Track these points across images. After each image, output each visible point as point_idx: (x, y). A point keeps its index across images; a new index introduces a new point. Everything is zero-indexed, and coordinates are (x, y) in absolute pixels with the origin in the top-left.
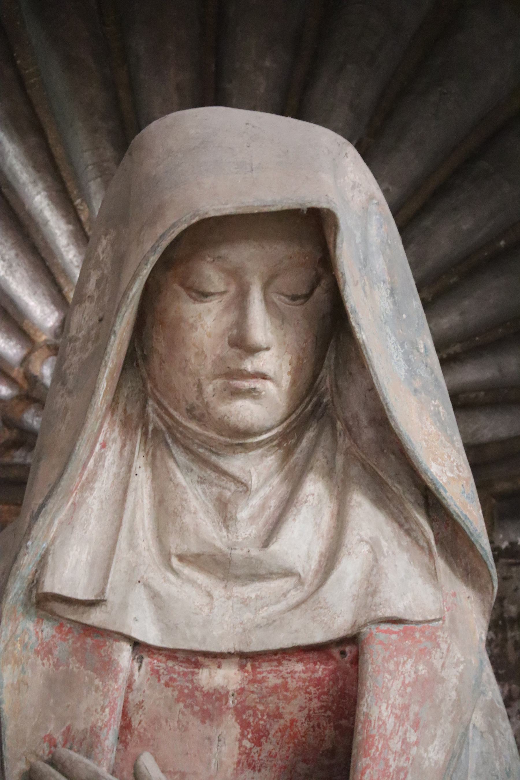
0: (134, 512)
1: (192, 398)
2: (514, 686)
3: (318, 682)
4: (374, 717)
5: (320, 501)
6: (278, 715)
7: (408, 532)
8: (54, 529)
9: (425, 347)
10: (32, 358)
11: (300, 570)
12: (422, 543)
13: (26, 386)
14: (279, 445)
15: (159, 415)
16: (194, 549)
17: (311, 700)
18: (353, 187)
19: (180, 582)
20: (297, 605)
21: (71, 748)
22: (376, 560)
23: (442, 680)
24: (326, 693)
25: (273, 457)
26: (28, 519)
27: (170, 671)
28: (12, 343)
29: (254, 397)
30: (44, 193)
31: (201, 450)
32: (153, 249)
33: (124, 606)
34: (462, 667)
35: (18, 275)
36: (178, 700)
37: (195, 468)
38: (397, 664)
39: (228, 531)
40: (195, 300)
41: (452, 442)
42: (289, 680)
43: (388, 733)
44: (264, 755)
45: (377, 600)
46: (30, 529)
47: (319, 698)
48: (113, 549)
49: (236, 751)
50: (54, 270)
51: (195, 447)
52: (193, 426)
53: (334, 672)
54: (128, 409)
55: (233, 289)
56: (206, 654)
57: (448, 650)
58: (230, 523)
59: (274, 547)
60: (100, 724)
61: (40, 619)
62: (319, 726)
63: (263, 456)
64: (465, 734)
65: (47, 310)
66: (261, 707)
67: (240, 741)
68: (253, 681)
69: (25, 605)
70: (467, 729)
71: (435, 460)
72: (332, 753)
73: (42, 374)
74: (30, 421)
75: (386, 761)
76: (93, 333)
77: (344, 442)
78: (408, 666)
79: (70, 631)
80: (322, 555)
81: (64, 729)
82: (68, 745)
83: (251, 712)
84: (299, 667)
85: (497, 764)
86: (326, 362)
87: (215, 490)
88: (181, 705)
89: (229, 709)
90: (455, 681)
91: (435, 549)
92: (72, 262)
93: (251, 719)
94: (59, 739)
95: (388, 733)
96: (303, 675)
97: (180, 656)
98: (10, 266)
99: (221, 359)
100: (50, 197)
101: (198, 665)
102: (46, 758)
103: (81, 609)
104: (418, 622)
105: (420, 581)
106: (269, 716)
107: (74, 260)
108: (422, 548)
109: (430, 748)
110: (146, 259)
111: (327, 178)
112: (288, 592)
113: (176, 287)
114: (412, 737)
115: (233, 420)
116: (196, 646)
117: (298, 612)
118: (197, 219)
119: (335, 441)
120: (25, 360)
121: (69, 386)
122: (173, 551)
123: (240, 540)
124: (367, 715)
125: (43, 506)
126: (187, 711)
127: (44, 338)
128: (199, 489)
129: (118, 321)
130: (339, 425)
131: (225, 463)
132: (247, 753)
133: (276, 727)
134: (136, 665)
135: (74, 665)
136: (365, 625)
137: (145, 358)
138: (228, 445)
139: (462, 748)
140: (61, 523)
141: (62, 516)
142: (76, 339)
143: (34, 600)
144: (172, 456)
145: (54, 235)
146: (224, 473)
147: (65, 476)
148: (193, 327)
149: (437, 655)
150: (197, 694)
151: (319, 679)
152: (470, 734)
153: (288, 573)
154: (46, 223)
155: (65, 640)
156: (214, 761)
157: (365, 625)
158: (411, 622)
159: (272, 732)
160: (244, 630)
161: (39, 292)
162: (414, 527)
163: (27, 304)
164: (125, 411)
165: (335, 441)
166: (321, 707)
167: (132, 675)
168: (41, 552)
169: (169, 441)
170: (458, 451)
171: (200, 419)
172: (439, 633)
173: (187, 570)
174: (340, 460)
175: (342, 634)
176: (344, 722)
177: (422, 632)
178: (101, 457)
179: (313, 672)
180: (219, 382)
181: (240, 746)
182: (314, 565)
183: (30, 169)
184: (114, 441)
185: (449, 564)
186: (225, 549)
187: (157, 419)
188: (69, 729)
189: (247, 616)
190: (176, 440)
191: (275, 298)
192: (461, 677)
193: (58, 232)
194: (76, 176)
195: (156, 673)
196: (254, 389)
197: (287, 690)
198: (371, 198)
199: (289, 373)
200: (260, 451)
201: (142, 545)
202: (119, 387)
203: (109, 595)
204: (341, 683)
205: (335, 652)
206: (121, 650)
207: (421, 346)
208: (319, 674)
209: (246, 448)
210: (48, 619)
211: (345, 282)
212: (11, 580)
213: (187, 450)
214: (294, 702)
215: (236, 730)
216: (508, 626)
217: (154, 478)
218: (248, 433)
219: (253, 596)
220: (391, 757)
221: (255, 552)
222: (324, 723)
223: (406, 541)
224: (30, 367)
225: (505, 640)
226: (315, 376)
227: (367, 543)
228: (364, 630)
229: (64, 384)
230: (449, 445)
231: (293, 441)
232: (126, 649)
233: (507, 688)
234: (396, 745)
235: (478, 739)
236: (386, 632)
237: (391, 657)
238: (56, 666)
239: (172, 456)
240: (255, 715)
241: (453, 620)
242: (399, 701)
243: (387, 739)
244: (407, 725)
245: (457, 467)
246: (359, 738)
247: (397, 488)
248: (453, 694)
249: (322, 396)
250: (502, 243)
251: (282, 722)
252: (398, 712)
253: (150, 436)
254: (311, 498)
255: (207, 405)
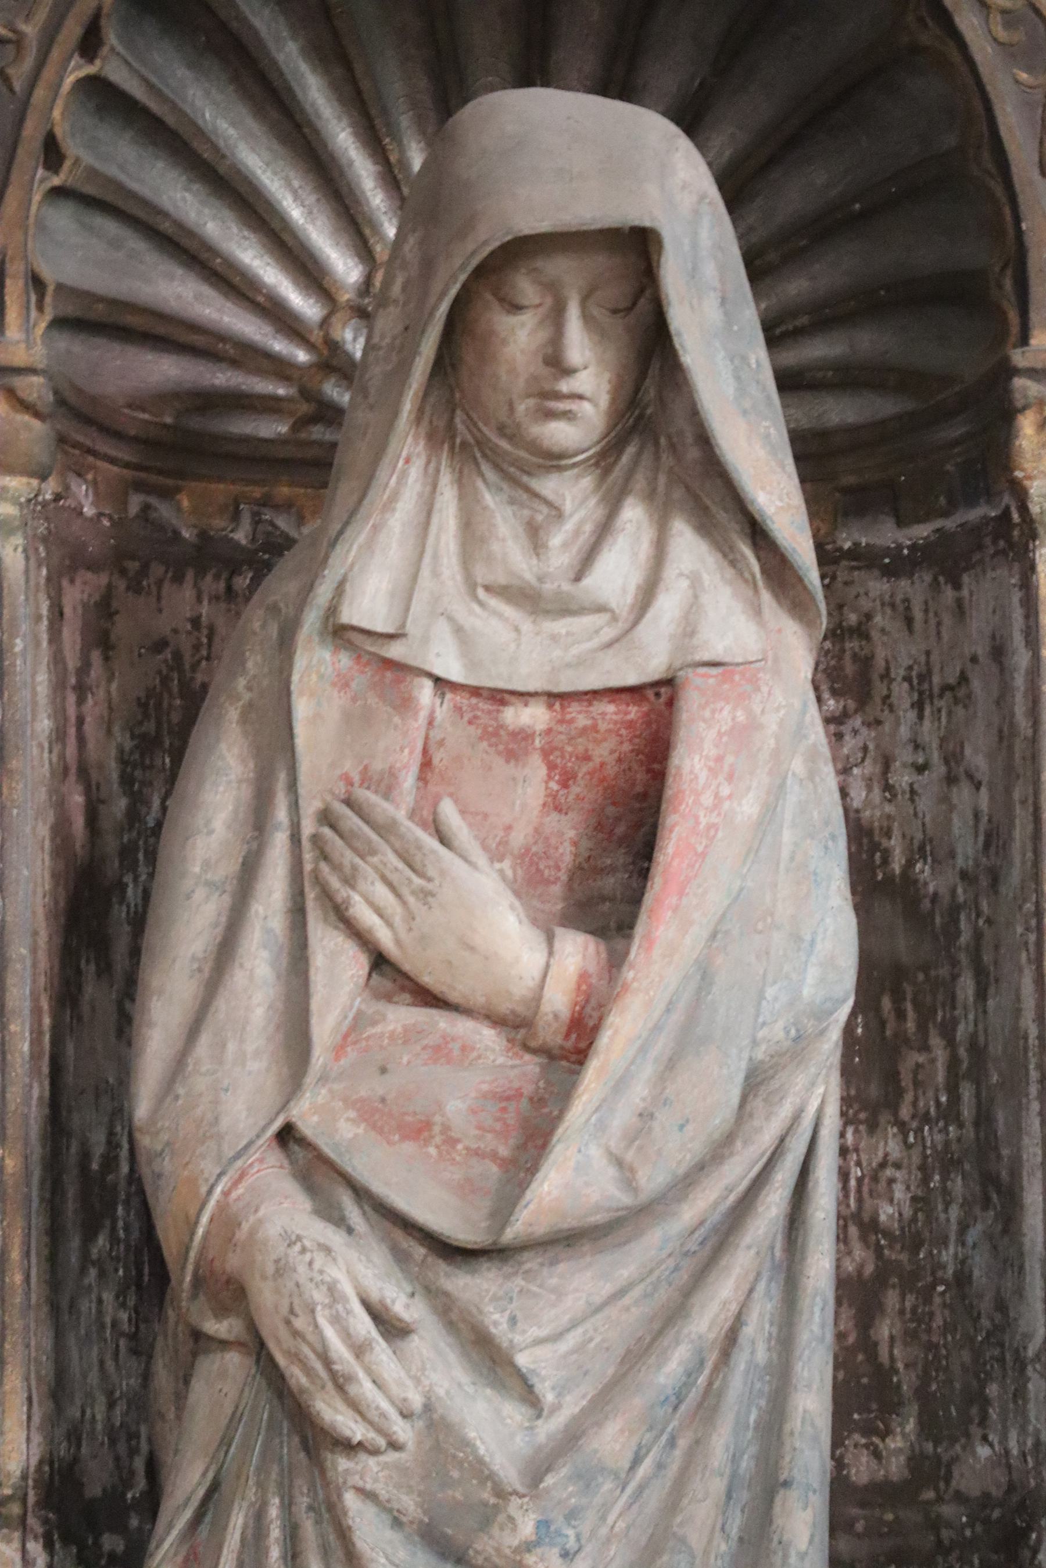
0: (438, 538)
1: (502, 415)
2: (850, 701)
3: (630, 725)
4: (686, 770)
5: (638, 529)
6: (587, 758)
7: (733, 563)
8: (353, 553)
9: (757, 362)
10: (334, 320)
11: (613, 605)
12: (747, 575)
13: (325, 352)
14: (597, 464)
15: (467, 427)
16: (502, 580)
17: (622, 743)
18: (683, 188)
19: (485, 614)
20: (609, 645)
21: (368, 788)
22: (696, 597)
23: (760, 727)
24: (639, 736)
25: (589, 478)
26: (325, 544)
27: (474, 708)
28: (312, 301)
29: (569, 419)
30: (349, 130)
31: (512, 470)
32: (462, 267)
33: (426, 640)
34: (783, 712)
35: (319, 223)
36: (481, 739)
37: (505, 486)
38: (713, 712)
39: (539, 559)
40: (509, 312)
41: (783, 466)
42: (600, 722)
43: (700, 788)
44: (571, 797)
45: (695, 641)
46: (326, 558)
47: (630, 741)
48: (415, 578)
49: (542, 793)
50: (360, 220)
51: (505, 466)
52: (504, 444)
53: (647, 714)
54: (434, 419)
55: (549, 301)
56: (513, 693)
57: (769, 693)
58: (541, 551)
59: (587, 582)
60: (398, 765)
61: (337, 649)
62: (630, 769)
63: (578, 477)
64: (782, 786)
65: (351, 263)
66: (569, 749)
67: (547, 782)
68: (561, 722)
69: (321, 634)
70: (785, 778)
71: (763, 488)
72: (644, 796)
73: (343, 339)
74: (329, 392)
75: (696, 818)
76: (398, 342)
77: (668, 461)
78: (725, 713)
79: (368, 663)
80: (639, 587)
81: (361, 768)
82: (366, 785)
83: (557, 753)
84: (611, 708)
85: (815, 814)
86: (650, 372)
87: (526, 512)
88: (485, 744)
89: (535, 749)
90: (774, 727)
91: (760, 583)
92: (379, 209)
93: (559, 761)
94: (356, 778)
95: (700, 788)
96: (615, 717)
97: (485, 693)
98: (310, 213)
99: (535, 379)
100: (356, 134)
101: (503, 703)
102: (342, 797)
103: (380, 641)
104: (738, 664)
105: (743, 618)
106: (577, 758)
107: (382, 205)
108: (746, 581)
109: (744, 802)
110: (454, 277)
111: (652, 189)
112: (601, 628)
113: (488, 296)
114: (725, 791)
115: (546, 443)
116: (501, 685)
117: (611, 652)
118: (509, 238)
119: (657, 458)
120: (325, 322)
121: (371, 400)
122: (479, 580)
123: (551, 570)
124: (679, 768)
125: (341, 532)
126: (492, 750)
127: (346, 297)
128: (509, 511)
129: (424, 340)
130: (663, 441)
131: (535, 484)
132: (554, 796)
133: (584, 769)
134: (438, 701)
135: (372, 700)
136: (681, 669)
137: (453, 366)
138: (540, 466)
139: (777, 799)
140: (360, 547)
141: (362, 538)
142: (380, 348)
143: (330, 628)
144: (482, 475)
145: (359, 176)
146: (536, 495)
147: (365, 502)
148: (504, 342)
149: (757, 698)
150: (502, 732)
151: (631, 721)
152: (789, 782)
153: (601, 609)
154: (351, 163)
155: (362, 672)
156: (518, 802)
157: (681, 669)
158: (731, 664)
159: (580, 775)
160: (553, 669)
161: (342, 243)
162: (738, 557)
163: (328, 257)
164: (431, 422)
165: (657, 458)
166: (632, 751)
167: (432, 713)
168: (339, 578)
169: (478, 455)
170: (789, 476)
171: (511, 438)
172: (761, 675)
173: (493, 602)
174: (662, 479)
175: (656, 677)
176: (656, 766)
177: (743, 674)
178: (404, 474)
179: (626, 713)
180: (531, 402)
181: (547, 788)
182: (629, 599)
183: (336, 104)
184: (418, 455)
185: (776, 596)
186: (533, 581)
187: (466, 432)
188: (366, 768)
189: (557, 653)
190: (485, 456)
191: (596, 312)
192: (781, 723)
193: (363, 173)
194: (385, 112)
195: (458, 709)
196: (570, 411)
197: (597, 732)
198: (702, 197)
199: (608, 392)
200: (576, 471)
201: (446, 573)
202: (426, 395)
203: (410, 628)
204: (654, 726)
205: (650, 693)
206: (422, 687)
207: (753, 362)
208: (632, 716)
209: (560, 469)
210: (346, 649)
211: (669, 304)
212: (307, 609)
213: (497, 467)
214: (605, 745)
215: (543, 771)
216: (847, 636)
217: (461, 497)
218: (561, 456)
219: (563, 631)
220: (702, 814)
221: (566, 587)
222: (635, 766)
223: (730, 572)
224: (331, 331)
225: (843, 651)
226: (637, 390)
227: (688, 577)
228: (681, 673)
229: (366, 397)
230: (779, 470)
231: (612, 459)
232: (428, 685)
233: (842, 703)
234: (707, 799)
235: (797, 788)
236: (703, 676)
237: (707, 703)
238: (354, 699)
239: (482, 475)
240: (563, 757)
241: (776, 660)
242: (714, 752)
243: (698, 794)
244: (721, 778)
245: (787, 494)
246: (669, 793)
247: (722, 516)
248: (772, 742)
249: (645, 408)
250: (857, 206)
251: (591, 764)
252: (711, 764)
253: (457, 450)
254: (628, 525)
255: (518, 426)
